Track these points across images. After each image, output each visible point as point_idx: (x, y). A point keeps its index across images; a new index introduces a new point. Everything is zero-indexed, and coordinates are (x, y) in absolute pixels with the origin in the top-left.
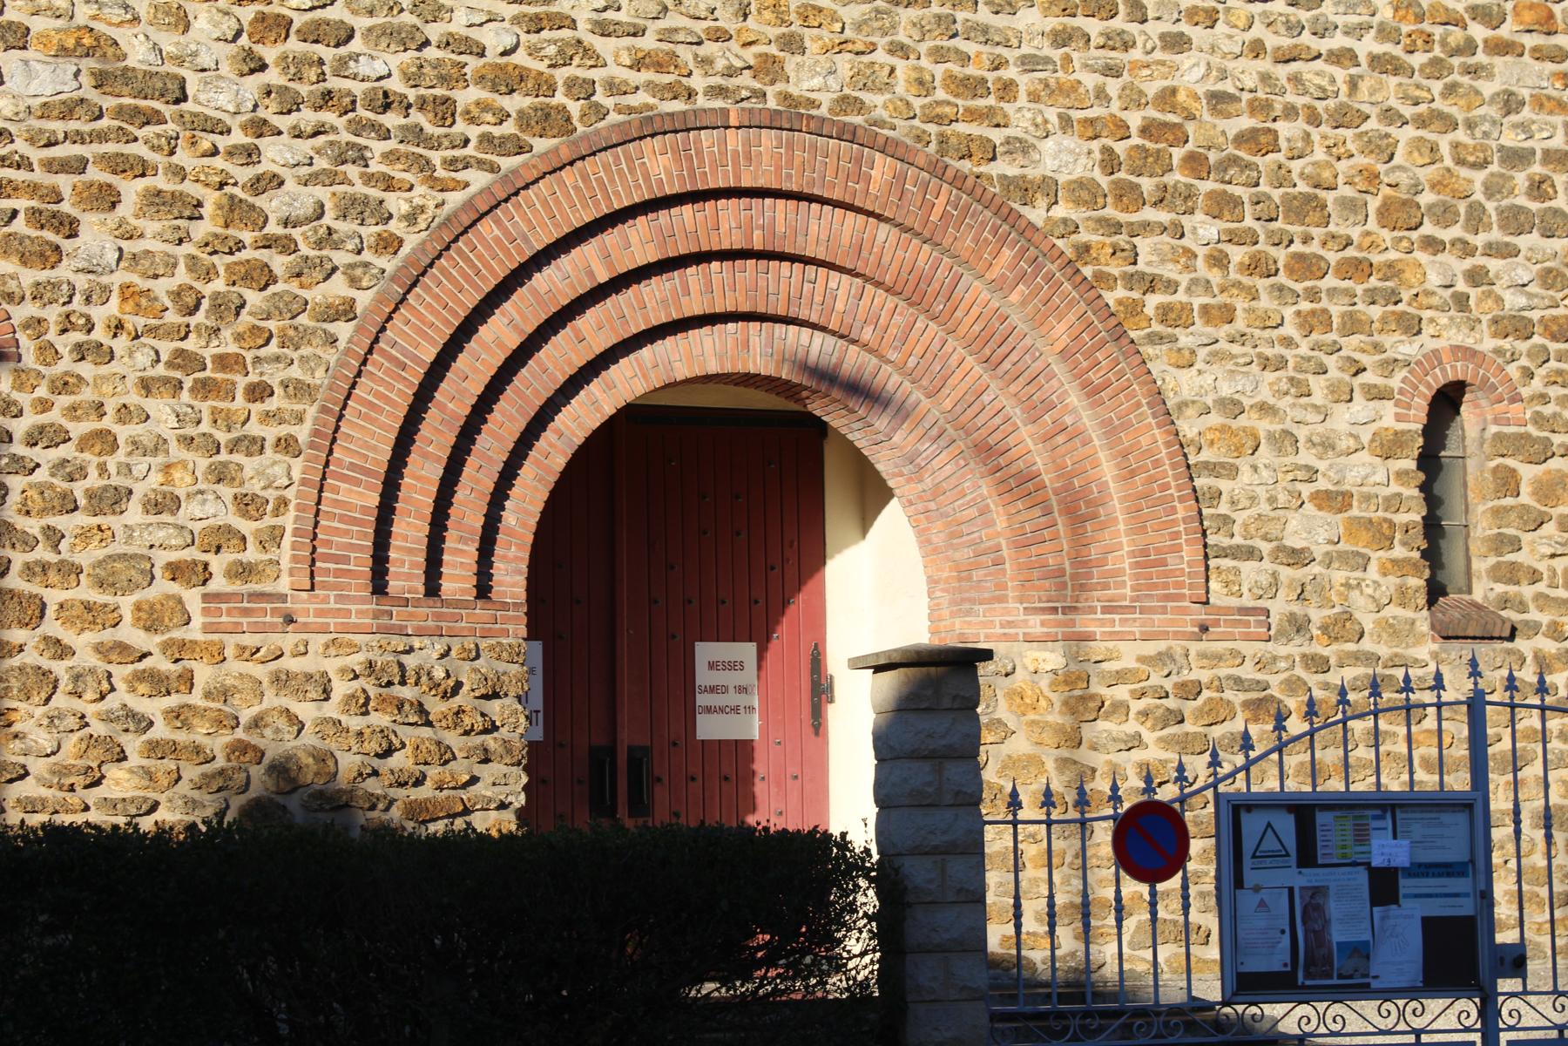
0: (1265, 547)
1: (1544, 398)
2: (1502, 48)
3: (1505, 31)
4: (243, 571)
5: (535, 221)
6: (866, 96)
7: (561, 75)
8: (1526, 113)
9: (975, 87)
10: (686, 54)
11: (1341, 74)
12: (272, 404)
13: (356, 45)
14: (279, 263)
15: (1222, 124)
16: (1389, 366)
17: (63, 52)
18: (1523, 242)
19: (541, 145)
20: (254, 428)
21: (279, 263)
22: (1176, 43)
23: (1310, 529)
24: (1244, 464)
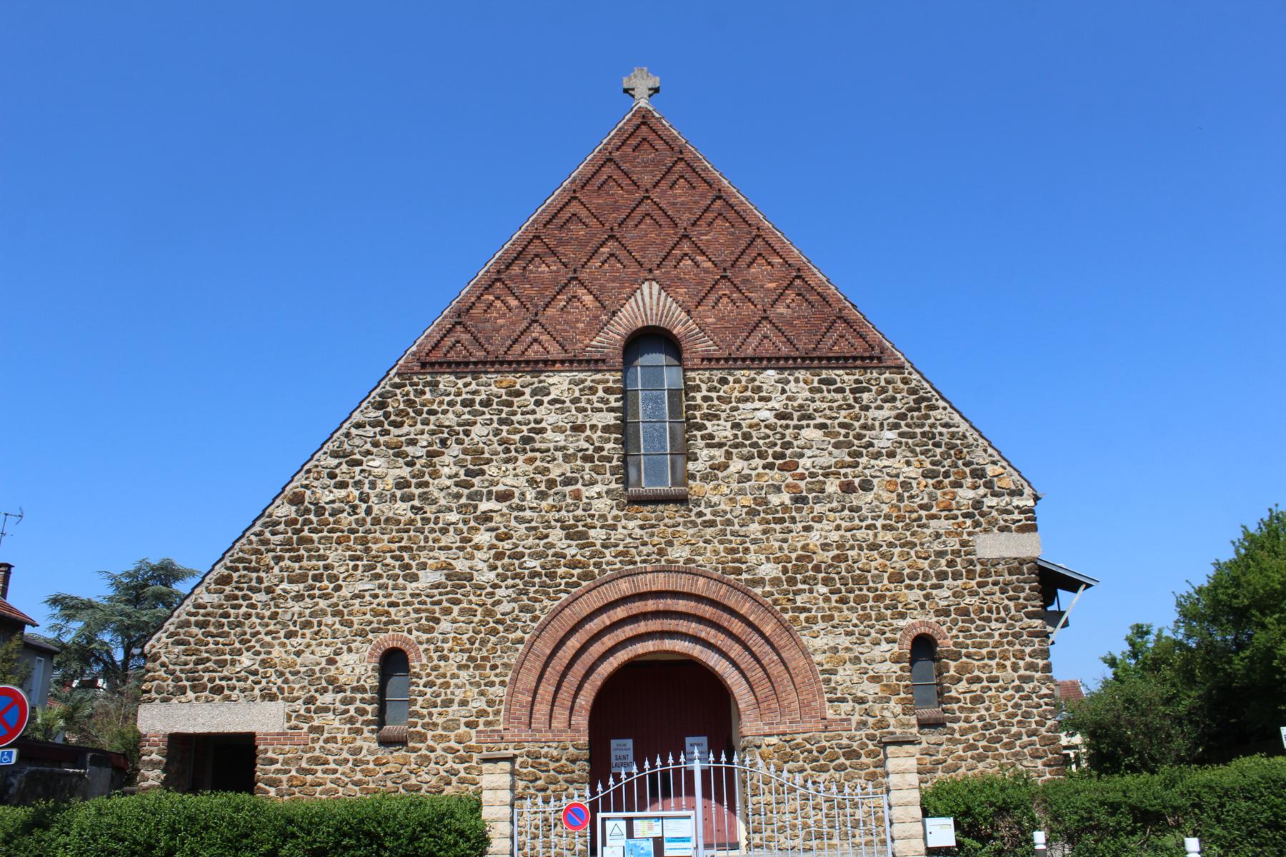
0: (849, 698)
1: (957, 637)
2: (933, 517)
3: (934, 511)
4: (488, 724)
5: (582, 608)
6: (697, 558)
7: (592, 561)
8: (944, 538)
9: (734, 551)
10: (633, 551)
11: (871, 533)
12: (498, 671)
13: (526, 558)
14: (501, 628)
15: (826, 554)
16: (894, 631)
17: (437, 569)
18: (945, 582)
19: (584, 584)
20: (493, 678)
21: (501, 628)
22: (807, 529)
23: (871, 689)
24: (840, 669)
